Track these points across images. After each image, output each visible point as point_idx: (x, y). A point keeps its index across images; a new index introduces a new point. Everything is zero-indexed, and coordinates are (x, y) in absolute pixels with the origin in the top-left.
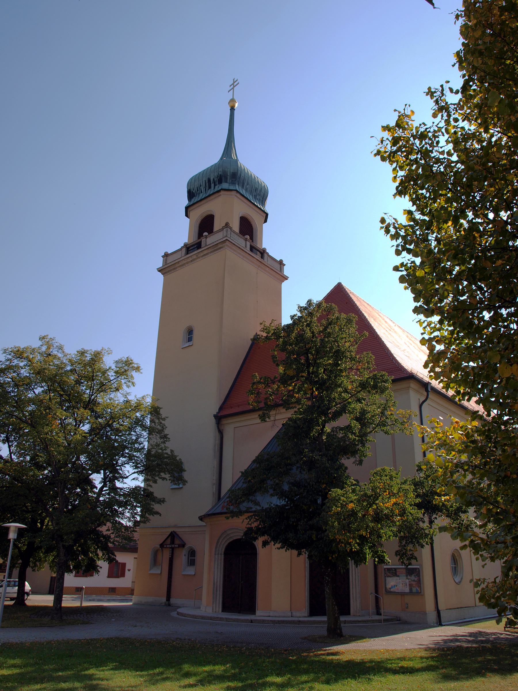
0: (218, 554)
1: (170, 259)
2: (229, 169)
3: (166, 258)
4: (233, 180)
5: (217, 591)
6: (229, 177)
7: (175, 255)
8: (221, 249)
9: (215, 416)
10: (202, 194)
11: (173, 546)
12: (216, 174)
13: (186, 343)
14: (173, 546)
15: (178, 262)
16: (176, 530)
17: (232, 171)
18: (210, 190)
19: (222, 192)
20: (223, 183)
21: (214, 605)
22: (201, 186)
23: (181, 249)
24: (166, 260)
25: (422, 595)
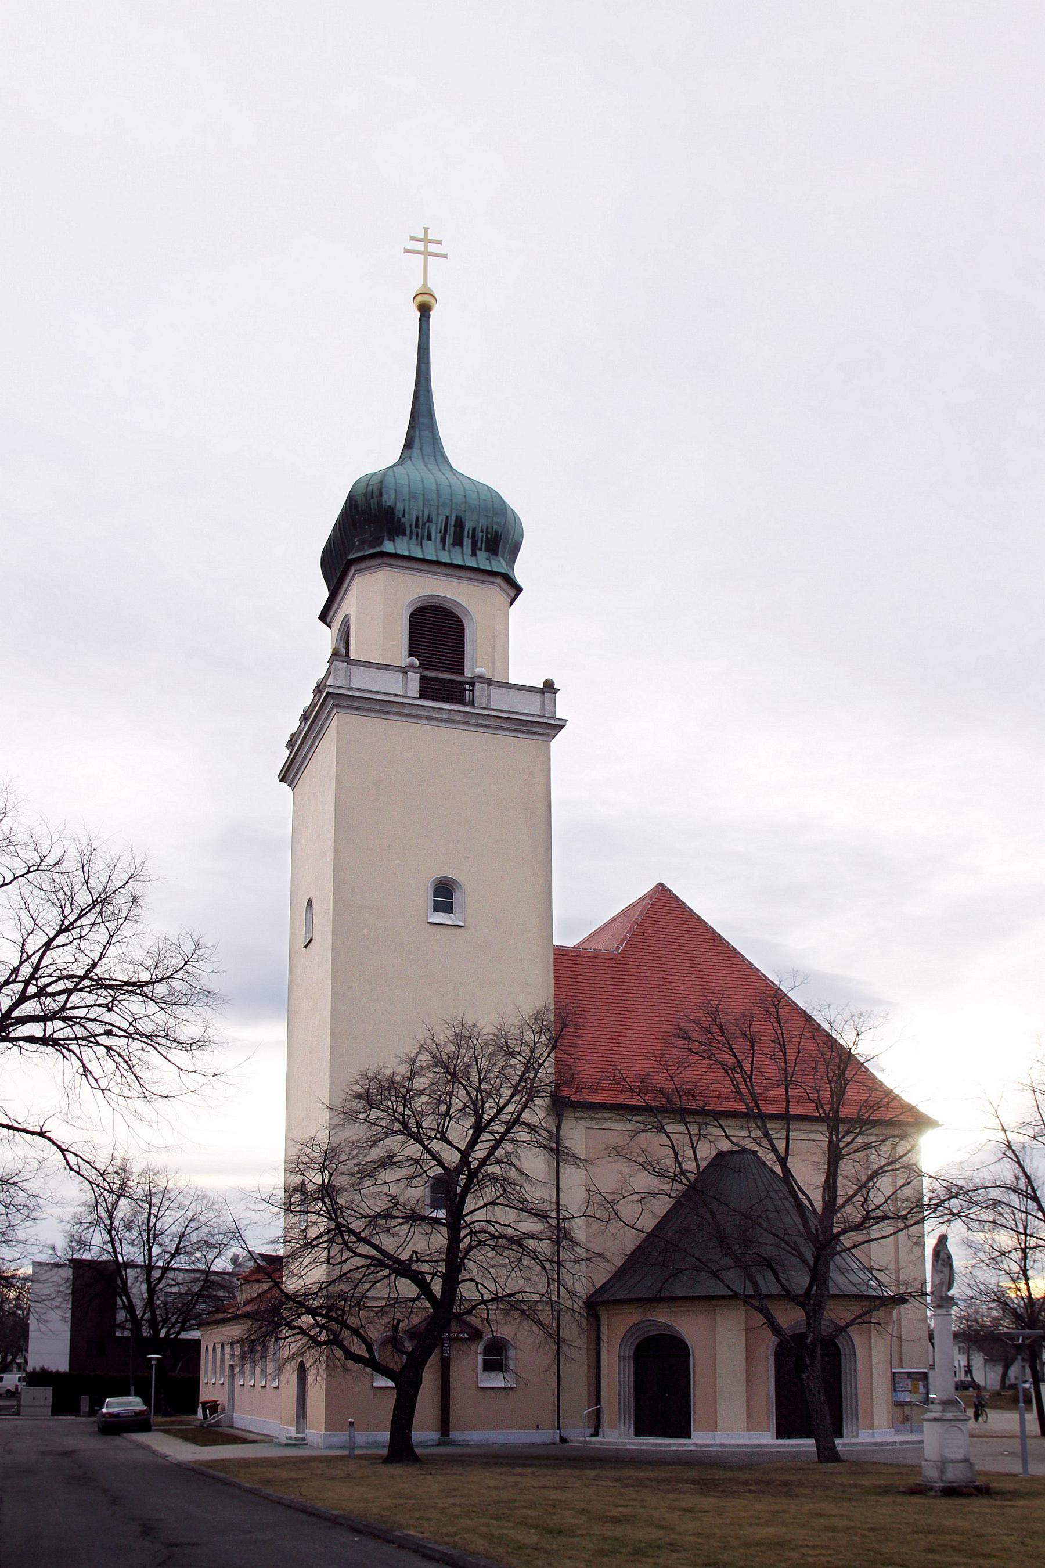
12: (483, 522)
19: (499, 580)
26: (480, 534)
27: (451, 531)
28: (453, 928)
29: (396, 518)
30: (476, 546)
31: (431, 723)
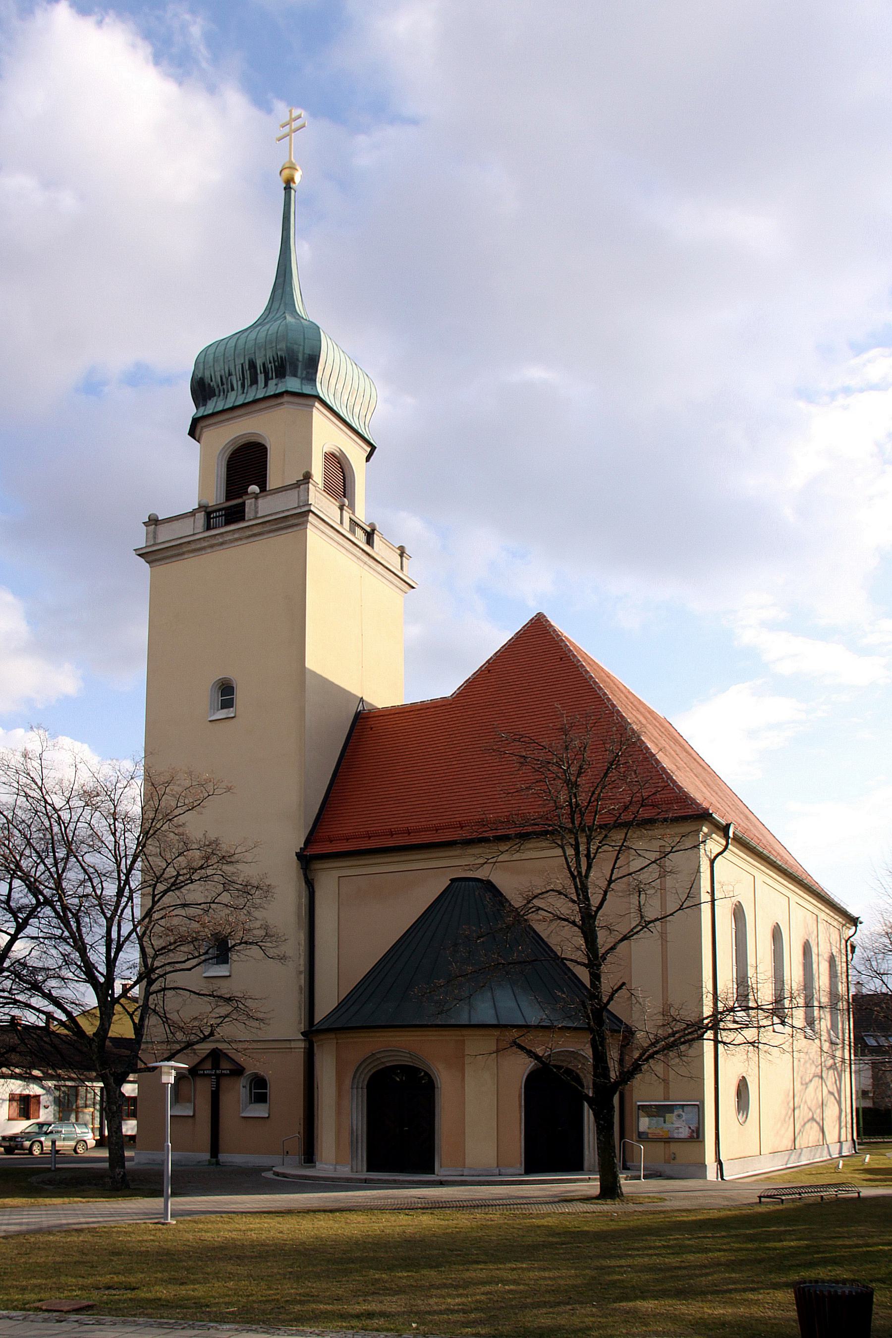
0: (357, 1088)
1: (166, 535)
2: (301, 348)
3: (155, 529)
4: (311, 371)
5: (357, 1142)
6: (300, 365)
7: (176, 525)
8: (295, 529)
9: (299, 856)
10: (234, 393)
11: (218, 1072)
12: (270, 354)
13: (218, 710)
14: (218, 1072)
15: (189, 542)
16: (220, 1046)
17: (307, 351)
18: (254, 387)
19: (286, 398)
20: (287, 377)
21: (354, 1163)
22: (230, 374)
23: (193, 513)
24: (155, 533)
25: (701, 1141)
26: (269, 366)
27: (248, 374)
28: (226, 720)
29: (207, 386)
30: (268, 376)
31: (214, 549)
